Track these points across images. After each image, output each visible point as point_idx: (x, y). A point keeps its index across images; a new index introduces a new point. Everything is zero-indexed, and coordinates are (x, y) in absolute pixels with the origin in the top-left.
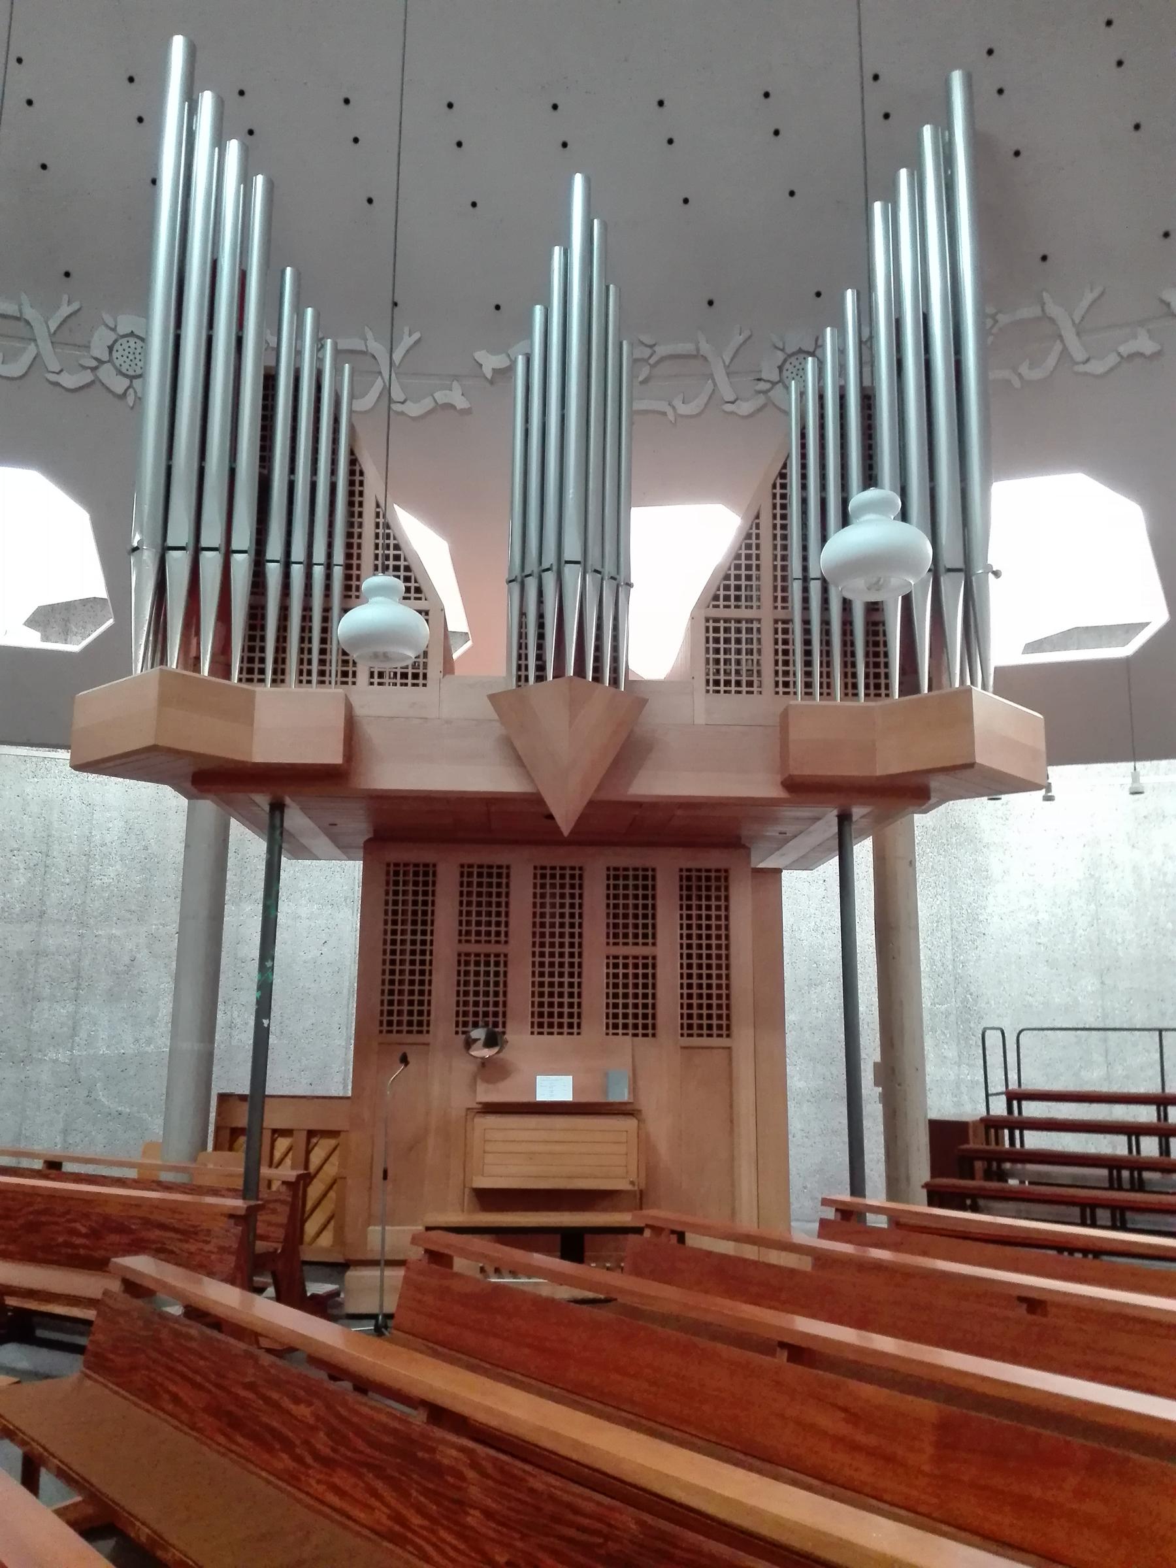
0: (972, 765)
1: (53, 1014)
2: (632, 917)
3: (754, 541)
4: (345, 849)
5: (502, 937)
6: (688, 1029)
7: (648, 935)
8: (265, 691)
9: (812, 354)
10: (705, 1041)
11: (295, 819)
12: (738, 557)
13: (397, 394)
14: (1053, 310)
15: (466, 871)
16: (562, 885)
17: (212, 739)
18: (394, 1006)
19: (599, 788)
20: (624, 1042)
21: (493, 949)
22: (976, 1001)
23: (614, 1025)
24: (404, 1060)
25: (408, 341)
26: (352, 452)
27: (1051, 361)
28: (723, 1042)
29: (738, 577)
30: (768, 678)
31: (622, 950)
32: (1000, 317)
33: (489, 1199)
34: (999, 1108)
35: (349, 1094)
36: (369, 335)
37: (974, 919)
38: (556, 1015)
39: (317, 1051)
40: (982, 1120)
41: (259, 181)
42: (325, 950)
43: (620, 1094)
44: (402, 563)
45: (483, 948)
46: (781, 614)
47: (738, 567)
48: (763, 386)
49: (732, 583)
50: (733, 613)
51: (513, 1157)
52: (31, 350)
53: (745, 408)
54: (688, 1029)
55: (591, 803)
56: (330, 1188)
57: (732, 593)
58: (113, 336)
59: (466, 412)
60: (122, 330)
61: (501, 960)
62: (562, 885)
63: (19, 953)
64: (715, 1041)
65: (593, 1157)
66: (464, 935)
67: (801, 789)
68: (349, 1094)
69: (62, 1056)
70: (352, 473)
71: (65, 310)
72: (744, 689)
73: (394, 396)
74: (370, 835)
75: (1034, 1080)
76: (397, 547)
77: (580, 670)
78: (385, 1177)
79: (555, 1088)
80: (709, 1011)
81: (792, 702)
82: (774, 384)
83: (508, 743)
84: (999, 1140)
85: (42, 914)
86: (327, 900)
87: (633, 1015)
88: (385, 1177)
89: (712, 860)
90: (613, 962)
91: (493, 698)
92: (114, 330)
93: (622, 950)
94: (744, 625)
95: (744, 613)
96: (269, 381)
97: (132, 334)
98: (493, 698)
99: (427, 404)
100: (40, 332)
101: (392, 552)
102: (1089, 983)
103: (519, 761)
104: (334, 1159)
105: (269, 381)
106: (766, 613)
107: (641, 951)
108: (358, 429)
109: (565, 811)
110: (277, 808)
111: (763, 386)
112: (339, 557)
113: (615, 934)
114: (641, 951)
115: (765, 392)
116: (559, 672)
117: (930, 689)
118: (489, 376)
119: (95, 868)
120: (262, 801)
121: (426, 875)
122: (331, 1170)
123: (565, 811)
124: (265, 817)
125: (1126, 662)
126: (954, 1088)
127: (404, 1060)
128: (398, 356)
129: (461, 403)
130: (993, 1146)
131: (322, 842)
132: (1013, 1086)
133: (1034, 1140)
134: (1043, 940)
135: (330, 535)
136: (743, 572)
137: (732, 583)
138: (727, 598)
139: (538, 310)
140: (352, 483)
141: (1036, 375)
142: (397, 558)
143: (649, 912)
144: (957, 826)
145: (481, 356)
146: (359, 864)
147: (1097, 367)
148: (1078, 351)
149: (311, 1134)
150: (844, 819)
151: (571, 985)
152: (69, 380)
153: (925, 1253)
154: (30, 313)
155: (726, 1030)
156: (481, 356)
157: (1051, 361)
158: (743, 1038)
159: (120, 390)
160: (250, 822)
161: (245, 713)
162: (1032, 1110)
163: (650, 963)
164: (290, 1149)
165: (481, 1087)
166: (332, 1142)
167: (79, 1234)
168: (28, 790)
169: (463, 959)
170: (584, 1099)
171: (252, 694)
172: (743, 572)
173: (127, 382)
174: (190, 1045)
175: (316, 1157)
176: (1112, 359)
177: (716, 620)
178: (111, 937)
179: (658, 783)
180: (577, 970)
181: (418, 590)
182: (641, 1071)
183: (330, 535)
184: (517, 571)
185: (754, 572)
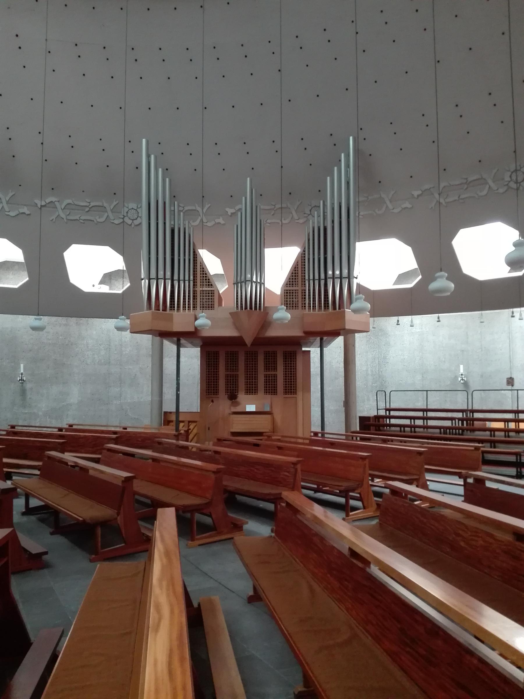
0: (345, 329)
1: (115, 391)
2: (271, 365)
3: (297, 269)
4: (195, 345)
5: (237, 370)
6: (286, 393)
7: (275, 369)
8: (175, 313)
9: (134, 495)
10: (290, 396)
11: (183, 341)
12: (290, 279)
13: (205, 220)
14: (383, 196)
15: (227, 353)
16: (251, 357)
17: (164, 327)
18: (209, 388)
19: (258, 334)
20: (269, 396)
21: (235, 373)
22: (385, 382)
23: (266, 392)
24: (212, 401)
25: (207, 206)
26: (194, 249)
27: (384, 209)
28: (295, 396)
29: (292, 279)
30: (300, 305)
31: (268, 373)
32: (369, 197)
33: (234, 434)
34: (382, 413)
35: (199, 411)
36: (197, 206)
37: (385, 358)
38: (251, 390)
39: (191, 401)
40: (375, 416)
41: (167, 180)
42: (190, 371)
43: (267, 409)
44: (207, 278)
45: (232, 373)
46: (303, 288)
47: (292, 276)
48: (306, 215)
49: (291, 280)
50: (291, 288)
51: (240, 424)
52: (106, 215)
53: (301, 221)
54: (286, 393)
55: (255, 338)
56: (195, 436)
57: (291, 283)
58: (128, 209)
59: (224, 224)
60: (130, 208)
61: (237, 376)
62: (251, 357)
63: (104, 374)
64: (292, 396)
65: (261, 424)
66: (227, 370)
67: (306, 333)
68: (199, 411)
69: (118, 402)
70: (194, 255)
71: (115, 203)
72: (294, 308)
73: (204, 221)
74: (202, 344)
75: (393, 406)
76: (206, 274)
77: (251, 308)
78: (209, 429)
79: (251, 408)
80: (291, 388)
81: (305, 312)
82: (309, 215)
83: (234, 324)
84: (379, 421)
85: (110, 362)
86: (192, 357)
87: (271, 389)
88: (209, 429)
89: (290, 349)
90: (266, 376)
91: (230, 313)
92: (128, 208)
93: (268, 373)
94: (294, 291)
95: (294, 288)
96: (173, 231)
97: (133, 209)
98: (230, 313)
99: (213, 223)
100: (108, 209)
101: (205, 275)
102: (419, 377)
103: (237, 328)
104: (196, 428)
105: (173, 231)
106: (299, 288)
107: (273, 373)
108: (195, 243)
109: (248, 341)
110: (179, 340)
111: (306, 215)
112: (192, 277)
113: (267, 368)
114: (273, 373)
115: (307, 217)
116: (246, 308)
117: (339, 309)
118: (230, 214)
119: (123, 349)
120: (175, 339)
121: (217, 354)
122: (195, 431)
123: (248, 341)
124: (176, 342)
125: (411, 288)
126: (367, 407)
127: (212, 401)
128: (204, 211)
129: (222, 222)
130: (377, 423)
131: (190, 345)
132: (388, 407)
133: (393, 421)
134: (405, 364)
135: (189, 271)
136: (294, 277)
137: (291, 280)
138: (290, 284)
139: (244, 198)
140: (194, 258)
141: (380, 212)
142: (206, 277)
143: (275, 363)
144: (381, 330)
145: (227, 209)
146: (199, 349)
147: (396, 211)
148: (390, 206)
149: (189, 422)
150: (321, 339)
151: (255, 382)
152: (117, 222)
153: (355, 451)
154: (105, 205)
155: (295, 393)
156: (227, 209)
157: (384, 209)
158: (300, 395)
159: (130, 224)
160: (173, 342)
161: (170, 318)
162: (393, 413)
163: (275, 376)
164: (184, 426)
165: (232, 408)
166: (195, 424)
167: (139, 441)
168: (103, 327)
169: (227, 376)
170: (258, 410)
171: (172, 315)
172: (294, 277)
173: (131, 221)
174: (156, 398)
175: (191, 427)
176: (400, 209)
177: (287, 290)
178: (129, 369)
179: (272, 333)
180: (256, 378)
181: (211, 285)
182: (276, 404)
183: (189, 271)
184: (235, 282)
185: (297, 277)
